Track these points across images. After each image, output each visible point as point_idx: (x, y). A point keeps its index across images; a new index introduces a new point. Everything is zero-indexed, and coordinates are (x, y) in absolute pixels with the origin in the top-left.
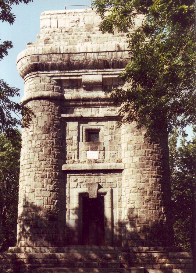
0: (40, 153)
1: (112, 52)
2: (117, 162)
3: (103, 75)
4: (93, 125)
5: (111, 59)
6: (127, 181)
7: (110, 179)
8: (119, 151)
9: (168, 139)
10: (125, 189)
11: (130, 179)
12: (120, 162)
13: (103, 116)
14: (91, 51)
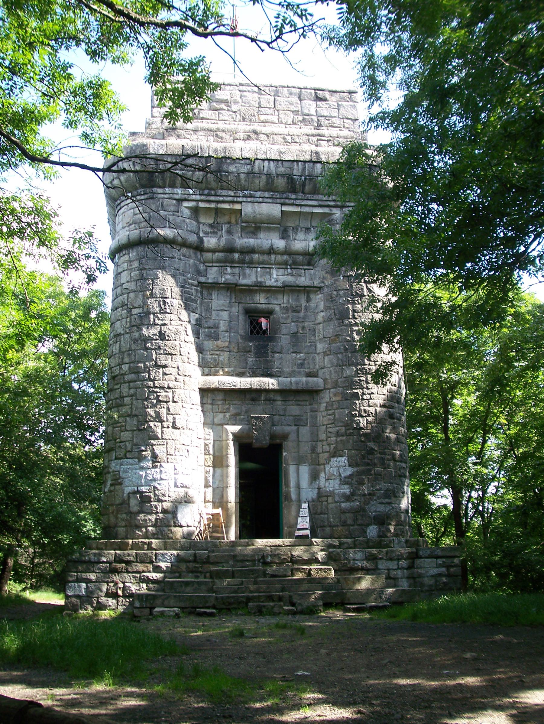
1: (305, 162)
2: (309, 375)
3: (282, 204)
4: (261, 301)
5: (301, 176)
9: (115, 619)
10: (327, 428)
11: (337, 409)
12: (316, 376)
13: (279, 284)
14: (263, 157)
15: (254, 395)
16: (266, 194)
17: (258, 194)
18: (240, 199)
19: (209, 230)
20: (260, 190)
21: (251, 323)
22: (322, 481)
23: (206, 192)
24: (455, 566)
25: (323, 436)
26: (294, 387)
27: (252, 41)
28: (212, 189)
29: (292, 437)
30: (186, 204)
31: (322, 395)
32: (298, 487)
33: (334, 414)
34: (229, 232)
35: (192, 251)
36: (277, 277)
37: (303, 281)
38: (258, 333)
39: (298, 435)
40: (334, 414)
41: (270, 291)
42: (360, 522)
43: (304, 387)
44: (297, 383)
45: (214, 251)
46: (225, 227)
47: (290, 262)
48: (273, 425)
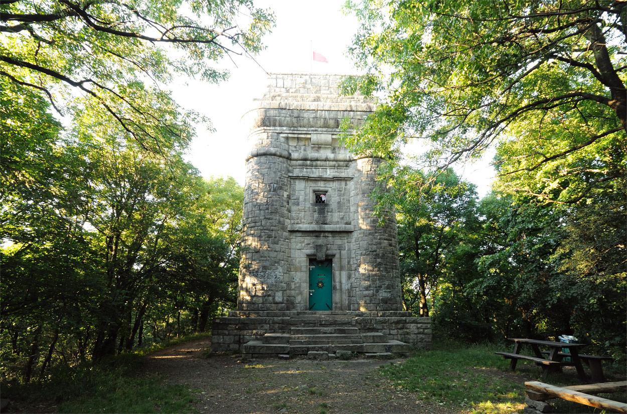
0: (266, 211)
2: (347, 224)
3: (332, 135)
4: (321, 186)
6: (357, 243)
7: (338, 241)
8: (347, 214)
12: (350, 224)
13: (331, 177)
14: (322, 109)
15: (317, 234)
16: (324, 129)
17: (320, 129)
18: (310, 132)
19: (294, 149)
20: (320, 127)
21: (316, 197)
22: (353, 280)
23: (292, 129)
24: (428, 328)
25: (353, 256)
26: (338, 230)
27: (327, 158)
28: (295, 127)
29: (337, 256)
30: (282, 135)
31: (353, 234)
32: (341, 282)
33: (359, 244)
34: (305, 150)
35: (285, 160)
36: (330, 173)
37: (343, 175)
38: (320, 202)
39: (340, 255)
40: (359, 244)
41: (326, 180)
42: (373, 302)
43: (344, 230)
44: (340, 228)
45: (296, 160)
46: (303, 148)
47: (337, 165)
48: (327, 250)
